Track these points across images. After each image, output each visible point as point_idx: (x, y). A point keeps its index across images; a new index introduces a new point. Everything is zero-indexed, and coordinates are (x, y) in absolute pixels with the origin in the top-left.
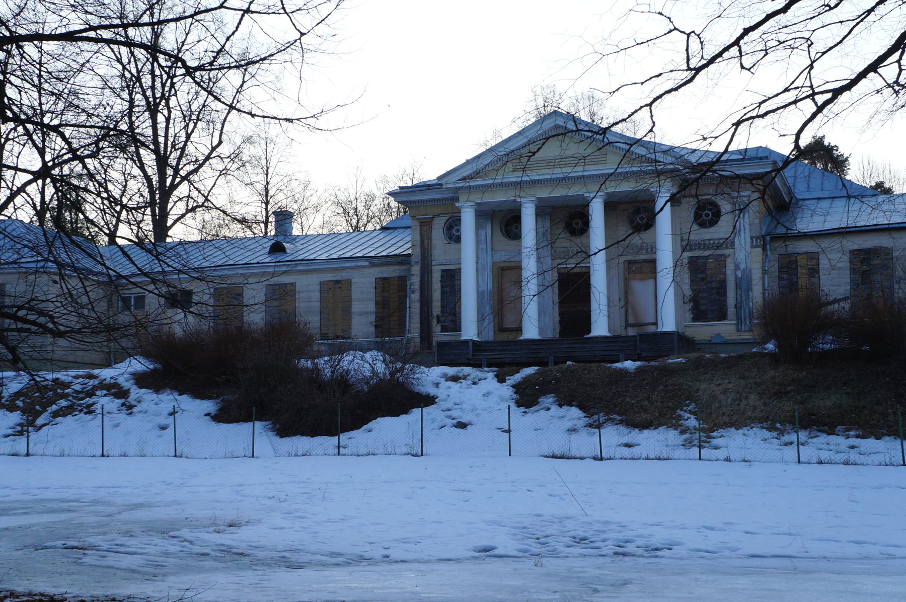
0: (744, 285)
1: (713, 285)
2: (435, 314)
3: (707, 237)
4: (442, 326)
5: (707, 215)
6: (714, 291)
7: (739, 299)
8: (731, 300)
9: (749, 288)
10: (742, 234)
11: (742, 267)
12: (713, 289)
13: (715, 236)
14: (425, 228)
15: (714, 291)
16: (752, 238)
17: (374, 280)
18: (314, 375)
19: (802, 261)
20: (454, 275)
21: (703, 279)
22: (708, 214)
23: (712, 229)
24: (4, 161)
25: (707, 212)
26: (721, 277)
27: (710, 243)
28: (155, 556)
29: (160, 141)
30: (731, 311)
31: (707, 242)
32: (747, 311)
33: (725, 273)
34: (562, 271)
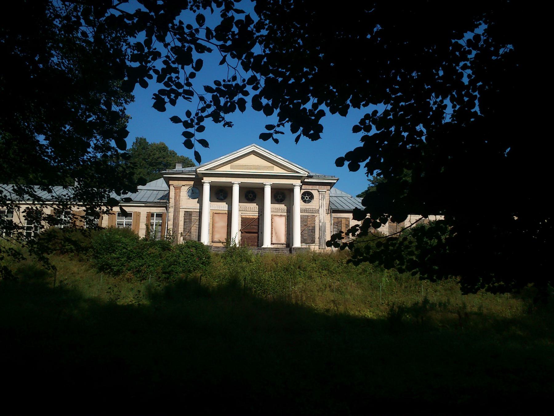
0: (322, 230)
1: (310, 228)
2: (180, 232)
3: (308, 207)
4: (183, 238)
5: (307, 198)
6: (310, 231)
7: (320, 235)
8: (317, 236)
9: (325, 231)
10: (322, 207)
11: (322, 221)
12: (310, 230)
13: (311, 207)
14: (178, 191)
15: (310, 231)
16: (326, 210)
17: (146, 213)
18: (430, 51)
19: (344, 221)
20: (191, 214)
21: (306, 225)
22: (307, 198)
23: (309, 204)
24: (410, 215)
25: (308, 199)
26: (313, 225)
27: (309, 210)
28: (167, 228)
29: (40, 135)
30: (317, 240)
31: (308, 210)
32: (324, 240)
33: (315, 224)
34: (243, 217)
